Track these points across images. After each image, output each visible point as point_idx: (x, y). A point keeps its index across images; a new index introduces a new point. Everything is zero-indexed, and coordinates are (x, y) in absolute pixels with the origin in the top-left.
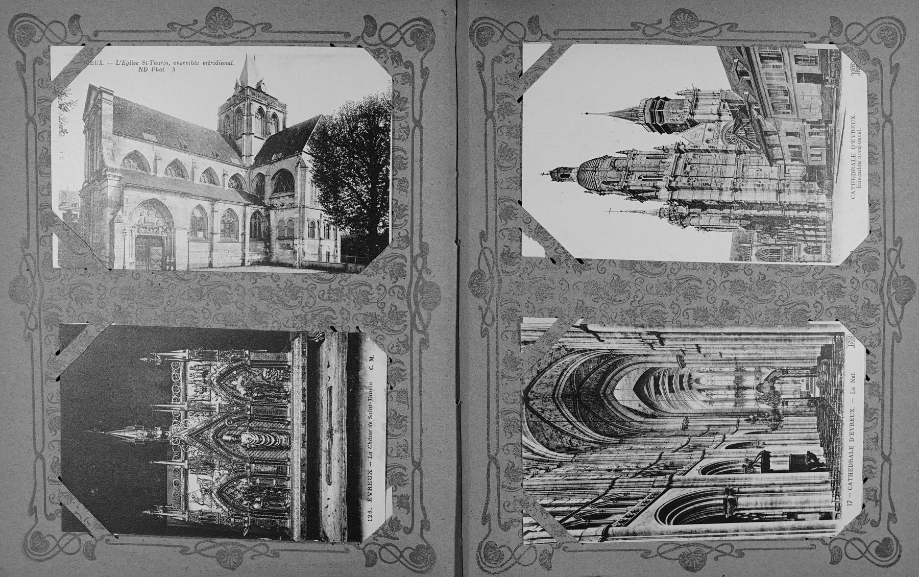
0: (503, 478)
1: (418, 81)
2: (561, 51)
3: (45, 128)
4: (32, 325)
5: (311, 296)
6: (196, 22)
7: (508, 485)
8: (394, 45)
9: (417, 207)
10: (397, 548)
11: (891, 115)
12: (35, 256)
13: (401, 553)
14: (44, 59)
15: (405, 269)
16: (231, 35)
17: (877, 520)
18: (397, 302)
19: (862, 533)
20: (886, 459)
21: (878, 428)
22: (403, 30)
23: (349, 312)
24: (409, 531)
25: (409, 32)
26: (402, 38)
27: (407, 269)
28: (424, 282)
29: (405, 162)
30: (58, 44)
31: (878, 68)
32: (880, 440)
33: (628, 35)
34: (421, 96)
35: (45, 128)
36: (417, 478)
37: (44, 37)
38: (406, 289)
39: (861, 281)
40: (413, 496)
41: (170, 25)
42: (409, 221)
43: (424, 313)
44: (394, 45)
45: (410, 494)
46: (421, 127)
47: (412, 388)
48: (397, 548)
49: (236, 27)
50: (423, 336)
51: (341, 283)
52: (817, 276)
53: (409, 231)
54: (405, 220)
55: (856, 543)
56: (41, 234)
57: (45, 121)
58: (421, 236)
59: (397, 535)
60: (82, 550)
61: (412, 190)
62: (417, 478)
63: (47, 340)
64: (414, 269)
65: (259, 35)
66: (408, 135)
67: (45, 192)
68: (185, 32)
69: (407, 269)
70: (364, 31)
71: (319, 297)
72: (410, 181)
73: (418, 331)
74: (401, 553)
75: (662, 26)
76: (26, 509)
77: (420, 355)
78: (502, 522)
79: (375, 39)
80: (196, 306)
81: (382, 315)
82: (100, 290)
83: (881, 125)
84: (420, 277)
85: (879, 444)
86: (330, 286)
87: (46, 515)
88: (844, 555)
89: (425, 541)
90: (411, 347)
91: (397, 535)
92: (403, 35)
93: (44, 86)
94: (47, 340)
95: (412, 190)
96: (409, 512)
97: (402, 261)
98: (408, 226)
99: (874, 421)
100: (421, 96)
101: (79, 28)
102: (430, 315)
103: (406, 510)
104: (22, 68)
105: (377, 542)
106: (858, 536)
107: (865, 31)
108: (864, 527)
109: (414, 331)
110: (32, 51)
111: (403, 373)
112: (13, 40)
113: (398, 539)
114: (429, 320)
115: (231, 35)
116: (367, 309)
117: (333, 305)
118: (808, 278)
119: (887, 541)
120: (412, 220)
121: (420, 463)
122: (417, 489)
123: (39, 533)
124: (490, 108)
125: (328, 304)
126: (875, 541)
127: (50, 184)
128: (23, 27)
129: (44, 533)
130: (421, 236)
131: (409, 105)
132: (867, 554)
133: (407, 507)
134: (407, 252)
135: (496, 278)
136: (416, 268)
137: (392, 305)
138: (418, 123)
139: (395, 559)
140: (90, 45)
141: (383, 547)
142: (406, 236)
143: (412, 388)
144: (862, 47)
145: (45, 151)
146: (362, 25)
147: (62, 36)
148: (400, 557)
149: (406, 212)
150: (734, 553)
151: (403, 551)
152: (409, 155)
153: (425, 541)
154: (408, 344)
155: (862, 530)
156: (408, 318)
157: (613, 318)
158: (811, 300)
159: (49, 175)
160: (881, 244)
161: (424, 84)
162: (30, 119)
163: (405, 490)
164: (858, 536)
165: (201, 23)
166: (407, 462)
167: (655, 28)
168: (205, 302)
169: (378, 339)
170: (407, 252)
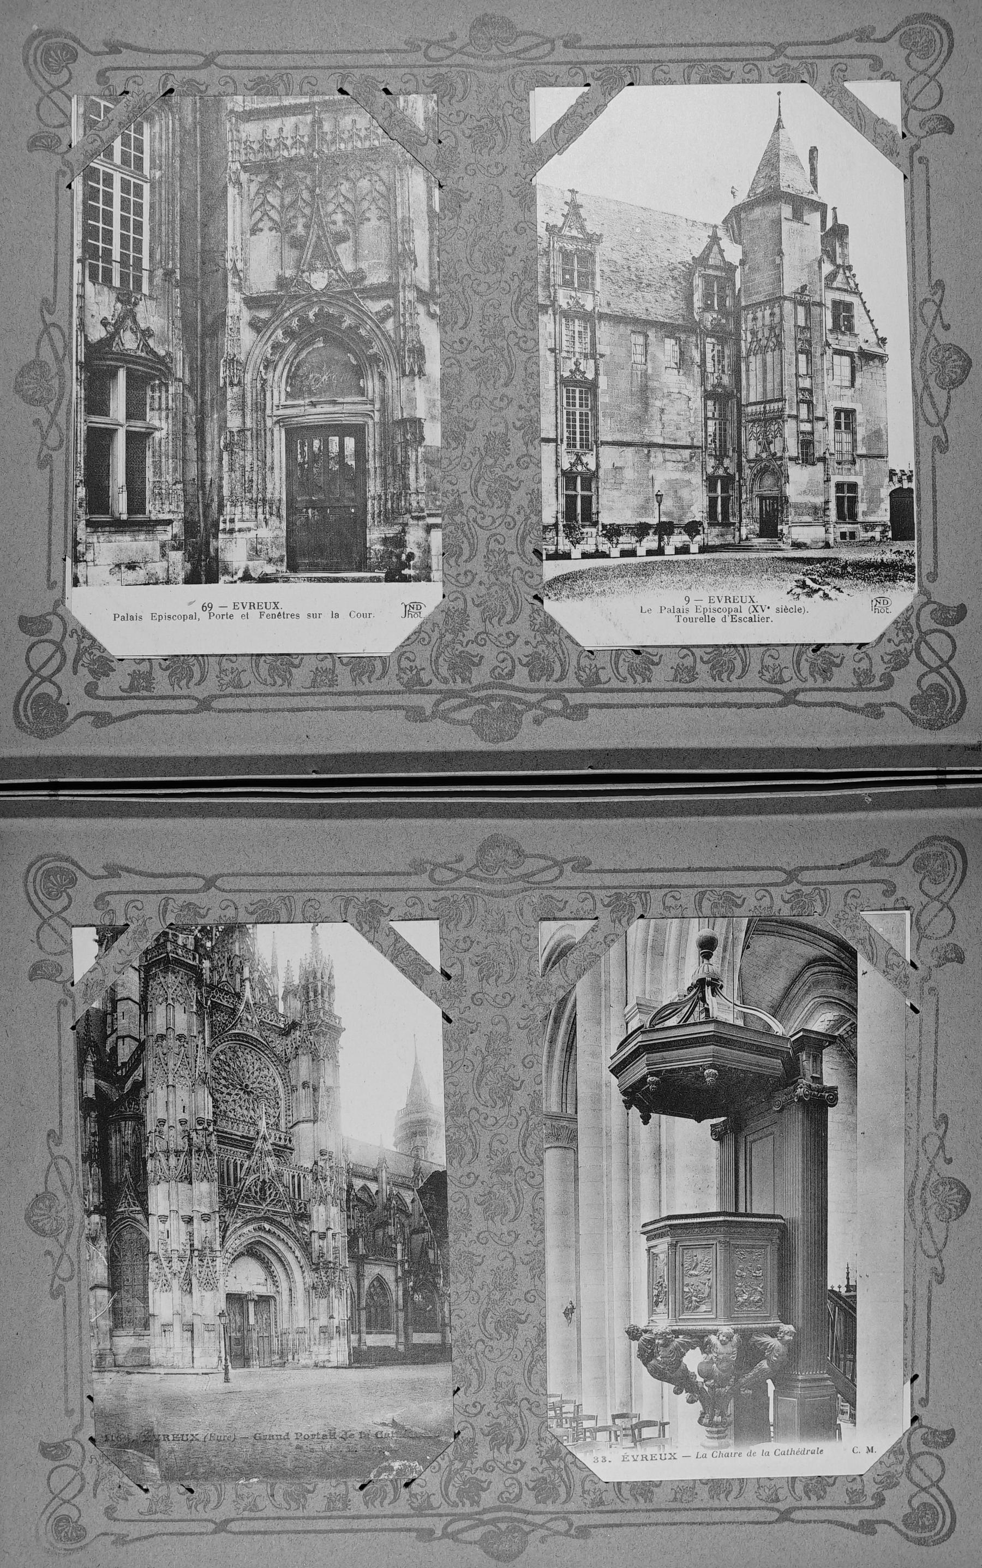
0: (182, 899)
1: (854, 1517)
2: (890, 153)
3: (766, 74)
4: (434, 53)
5: (494, 522)
6: (947, 327)
7: (170, 908)
8: (919, 657)
9: (648, 698)
10: (58, 670)
11: (799, 703)
12: (551, 59)
13: (49, 679)
14: (878, 70)
15: (549, 1502)
16: (926, 387)
17: (115, 1515)
18: (485, 668)
19: (95, 1490)
20: (222, 1527)
21: (257, 688)
22: (934, 1491)
23: (468, 585)
24: (110, 1512)
25: (932, 1501)
26: (932, 670)
27: (542, 684)
28: (520, 713)
29: (724, 676)
30: (904, 97)
31: (877, 683)
32: (239, 691)
33: (922, 272)
34: (832, 704)
35: (766, 74)
36: (184, 705)
37: (915, 74)
38: (509, 682)
39: (511, 650)
40: (151, 698)
41: (940, 284)
42: (622, 685)
43: (466, 714)
44: (919, 657)
45: (156, 692)
46: (782, 704)
47: (340, 694)
48: (58, 670)
49: (941, 396)
50: (428, 712)
51: (517, 572)
52: (513, 340)
53: (606, 686)
54: (625, 679)
55: (77, 1484)
56: (589, 69)
57: (776, 75)
58: (601, 706)
59: (83, 671)
60: (46, 129)
61: (678, 690)
62: (184, 705)
63: (409, 77)
64: (543, 695)
65: (929, 433)
66: (770, 682)
67: (659, 75)
68: (930, 310)
69: (542, 684)
70: (939, 604)
71: (495, 535)
72: (693, 685)
73: (437, 704)
74: (49, 679)
75: (938, 331)
76: (118, 37)
77: (397, 708)
78: (108, 898)
79: (927, 623)
80: (474, 328)
81: (460, 405)
82: (501, 400)
83: (779, 687)
84: (530, 706)
85: (246, 1514)
86: (512, 553)
87: (107, 69)
88: (57, 1463)
89: (75, 719)
90: (411, 692)
91: (83, 671)
92: (936, 670)
93: (836, 74)
94: (409, 77)
95: (678, 690)
96: (123, 691)
97: (557, 675)
98: (615, 684)
99: (269, 680)
100: (832, 704)
101: (932, 132)
102: (463, 723)
103: (126, 686)
104: (863, 35)
105: (86, 1463)
106: (70, 662)
107: (939, 663)
108: (86, 671)
109: (438, 696)
110: (893, 53)
111: (364, 679)
112: (908, 21)
113: (75, 673)
114: (454, 722)
115: (926, 387)
116: (475, 614)
117: (480, 557)
118: (521, 1392)
119: (80, 1533)
120: (623, 690)
121: (209, 708)
122: (185, 1527)
123: (74, 57)
124: (790, 51)
125: (482, 550)
126: (60, 693)
127: (672, 82)
128: (931, 42)
129: (75, 67)
130: (601, 706)
131: (820, 683)
132: (36, 680)
133: (132, 688)
134: (571, 682)
135: (503, 63)
136: (545, 699)
137: (482, 657)
138: (790, 699)
139: (35, 668)
140: (903, 147)
141: (59, 647)
142: (598, 681)
143: (340, 694)
144: (913, 657)
145: (728, 75)
146: (952, 601)
147: (919, 103)
148: (40, 677)
149: (639, 679)
150: (57, 1282)
151: (51, 682)
152: (735, 683)
153: (75, 719)
154: (415, 685)
155: (80, 668)
156: (460, 686)
157: (449, 478)
158: (477, 564)
159: (687, 81)
160: (575, 684)
161: (854, 709)
162: (779, 50)
163: (162, 683)
164: (89, 1488)
165: (944, 338)
166: (211, 686)
167: (935, 318)
168: (485, 579)
169: (423, 635)
170: (571, 682)
